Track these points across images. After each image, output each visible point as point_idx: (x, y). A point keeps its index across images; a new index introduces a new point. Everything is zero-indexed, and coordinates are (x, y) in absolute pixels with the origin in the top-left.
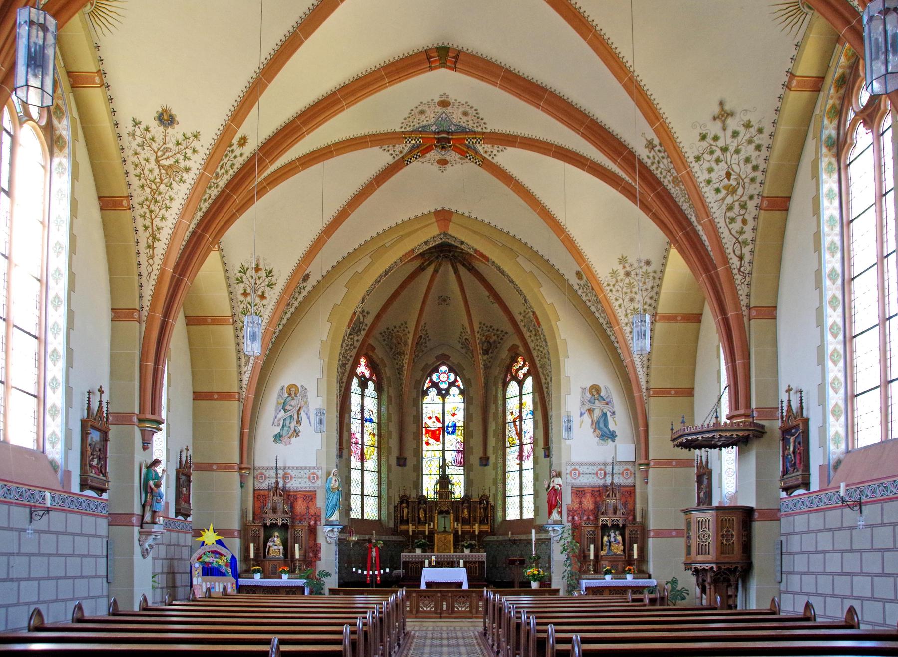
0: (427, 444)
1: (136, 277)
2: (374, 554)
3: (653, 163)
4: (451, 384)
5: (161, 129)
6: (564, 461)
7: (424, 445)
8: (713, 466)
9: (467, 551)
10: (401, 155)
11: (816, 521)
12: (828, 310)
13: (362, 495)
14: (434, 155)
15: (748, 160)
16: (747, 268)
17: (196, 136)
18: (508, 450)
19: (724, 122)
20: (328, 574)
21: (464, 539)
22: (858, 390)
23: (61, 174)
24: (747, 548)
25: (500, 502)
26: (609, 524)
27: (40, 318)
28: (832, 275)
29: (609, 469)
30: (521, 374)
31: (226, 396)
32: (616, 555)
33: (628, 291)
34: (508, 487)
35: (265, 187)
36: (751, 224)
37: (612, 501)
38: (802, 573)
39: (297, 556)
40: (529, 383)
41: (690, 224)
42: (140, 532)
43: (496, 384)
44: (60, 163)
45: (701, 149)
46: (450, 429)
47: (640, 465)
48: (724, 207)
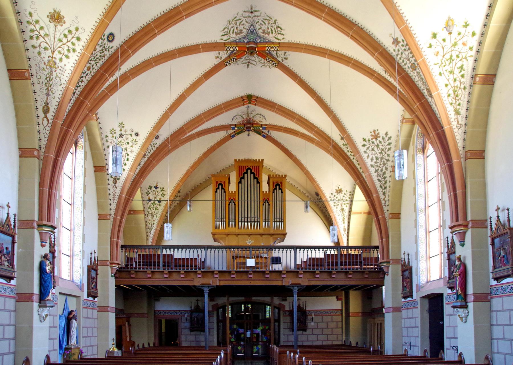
5: (52, 25)
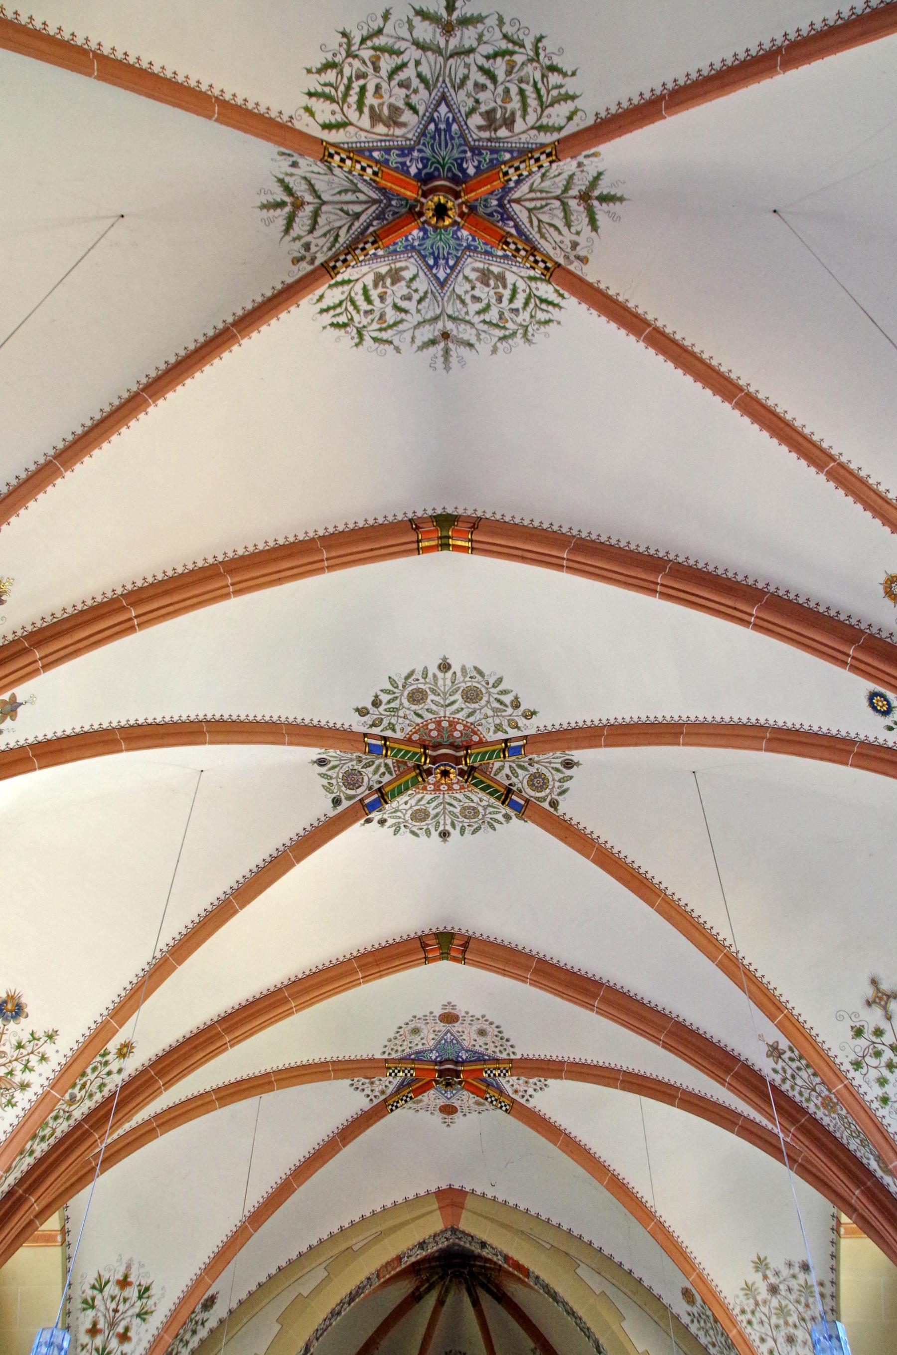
3: (784, 1080)
10: (383, 1097)
14: (433, 1097)
19: (885, 1007)
33: (781, 1322)
35: (154, 1129)
41: (870, 1174)
45: (858, 1049)
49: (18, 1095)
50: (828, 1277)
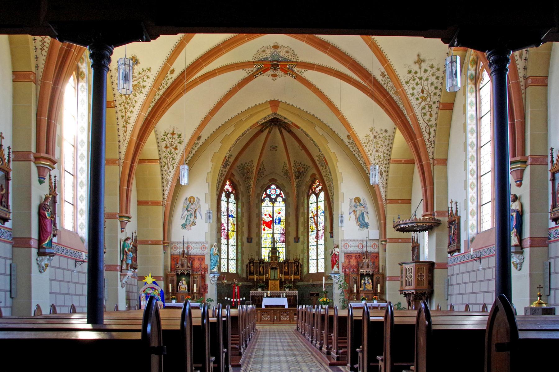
0: (264, 230)
1: (117, 143)
2: (236, 290)
3: (385, 84)
4: (278, 196)
6: (340, 239)
7: (262, 231)
8: (420, 242)
9: (287, 290)
11: (463, 268)
12: (469, 163)
13: (228, 259)
14: (271, 72)
15: (432, 84)
16: (432, 139)
17: (149, 70)
18: (310, 233)
19: (420, 65)
20: (212, 300)
21: (285, 282)
22: (483, 203)
23: (83, 91)
24: (431, 283)
25: (306, 263)
26: (365, 273)
27: (74, 165)
28: (472, 145)
29: (365, 243)
30: (317, 190)
31: (156, 203)
32: (368, 290)
34: (310, 254)
36: (434, 116)
37: (366, 261)
38: (456, 294)
39: (195, 291)
40: (322, 195)
41: (404, 115)
42: (121, 275)
43: (303, 196)
44: (82, 86)
46: (277, 221)
47: (382, 241)
48: (420, 107)
49: (143, 90)
50: (392, 134)
